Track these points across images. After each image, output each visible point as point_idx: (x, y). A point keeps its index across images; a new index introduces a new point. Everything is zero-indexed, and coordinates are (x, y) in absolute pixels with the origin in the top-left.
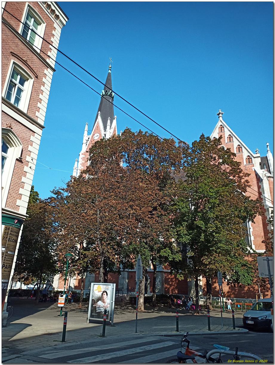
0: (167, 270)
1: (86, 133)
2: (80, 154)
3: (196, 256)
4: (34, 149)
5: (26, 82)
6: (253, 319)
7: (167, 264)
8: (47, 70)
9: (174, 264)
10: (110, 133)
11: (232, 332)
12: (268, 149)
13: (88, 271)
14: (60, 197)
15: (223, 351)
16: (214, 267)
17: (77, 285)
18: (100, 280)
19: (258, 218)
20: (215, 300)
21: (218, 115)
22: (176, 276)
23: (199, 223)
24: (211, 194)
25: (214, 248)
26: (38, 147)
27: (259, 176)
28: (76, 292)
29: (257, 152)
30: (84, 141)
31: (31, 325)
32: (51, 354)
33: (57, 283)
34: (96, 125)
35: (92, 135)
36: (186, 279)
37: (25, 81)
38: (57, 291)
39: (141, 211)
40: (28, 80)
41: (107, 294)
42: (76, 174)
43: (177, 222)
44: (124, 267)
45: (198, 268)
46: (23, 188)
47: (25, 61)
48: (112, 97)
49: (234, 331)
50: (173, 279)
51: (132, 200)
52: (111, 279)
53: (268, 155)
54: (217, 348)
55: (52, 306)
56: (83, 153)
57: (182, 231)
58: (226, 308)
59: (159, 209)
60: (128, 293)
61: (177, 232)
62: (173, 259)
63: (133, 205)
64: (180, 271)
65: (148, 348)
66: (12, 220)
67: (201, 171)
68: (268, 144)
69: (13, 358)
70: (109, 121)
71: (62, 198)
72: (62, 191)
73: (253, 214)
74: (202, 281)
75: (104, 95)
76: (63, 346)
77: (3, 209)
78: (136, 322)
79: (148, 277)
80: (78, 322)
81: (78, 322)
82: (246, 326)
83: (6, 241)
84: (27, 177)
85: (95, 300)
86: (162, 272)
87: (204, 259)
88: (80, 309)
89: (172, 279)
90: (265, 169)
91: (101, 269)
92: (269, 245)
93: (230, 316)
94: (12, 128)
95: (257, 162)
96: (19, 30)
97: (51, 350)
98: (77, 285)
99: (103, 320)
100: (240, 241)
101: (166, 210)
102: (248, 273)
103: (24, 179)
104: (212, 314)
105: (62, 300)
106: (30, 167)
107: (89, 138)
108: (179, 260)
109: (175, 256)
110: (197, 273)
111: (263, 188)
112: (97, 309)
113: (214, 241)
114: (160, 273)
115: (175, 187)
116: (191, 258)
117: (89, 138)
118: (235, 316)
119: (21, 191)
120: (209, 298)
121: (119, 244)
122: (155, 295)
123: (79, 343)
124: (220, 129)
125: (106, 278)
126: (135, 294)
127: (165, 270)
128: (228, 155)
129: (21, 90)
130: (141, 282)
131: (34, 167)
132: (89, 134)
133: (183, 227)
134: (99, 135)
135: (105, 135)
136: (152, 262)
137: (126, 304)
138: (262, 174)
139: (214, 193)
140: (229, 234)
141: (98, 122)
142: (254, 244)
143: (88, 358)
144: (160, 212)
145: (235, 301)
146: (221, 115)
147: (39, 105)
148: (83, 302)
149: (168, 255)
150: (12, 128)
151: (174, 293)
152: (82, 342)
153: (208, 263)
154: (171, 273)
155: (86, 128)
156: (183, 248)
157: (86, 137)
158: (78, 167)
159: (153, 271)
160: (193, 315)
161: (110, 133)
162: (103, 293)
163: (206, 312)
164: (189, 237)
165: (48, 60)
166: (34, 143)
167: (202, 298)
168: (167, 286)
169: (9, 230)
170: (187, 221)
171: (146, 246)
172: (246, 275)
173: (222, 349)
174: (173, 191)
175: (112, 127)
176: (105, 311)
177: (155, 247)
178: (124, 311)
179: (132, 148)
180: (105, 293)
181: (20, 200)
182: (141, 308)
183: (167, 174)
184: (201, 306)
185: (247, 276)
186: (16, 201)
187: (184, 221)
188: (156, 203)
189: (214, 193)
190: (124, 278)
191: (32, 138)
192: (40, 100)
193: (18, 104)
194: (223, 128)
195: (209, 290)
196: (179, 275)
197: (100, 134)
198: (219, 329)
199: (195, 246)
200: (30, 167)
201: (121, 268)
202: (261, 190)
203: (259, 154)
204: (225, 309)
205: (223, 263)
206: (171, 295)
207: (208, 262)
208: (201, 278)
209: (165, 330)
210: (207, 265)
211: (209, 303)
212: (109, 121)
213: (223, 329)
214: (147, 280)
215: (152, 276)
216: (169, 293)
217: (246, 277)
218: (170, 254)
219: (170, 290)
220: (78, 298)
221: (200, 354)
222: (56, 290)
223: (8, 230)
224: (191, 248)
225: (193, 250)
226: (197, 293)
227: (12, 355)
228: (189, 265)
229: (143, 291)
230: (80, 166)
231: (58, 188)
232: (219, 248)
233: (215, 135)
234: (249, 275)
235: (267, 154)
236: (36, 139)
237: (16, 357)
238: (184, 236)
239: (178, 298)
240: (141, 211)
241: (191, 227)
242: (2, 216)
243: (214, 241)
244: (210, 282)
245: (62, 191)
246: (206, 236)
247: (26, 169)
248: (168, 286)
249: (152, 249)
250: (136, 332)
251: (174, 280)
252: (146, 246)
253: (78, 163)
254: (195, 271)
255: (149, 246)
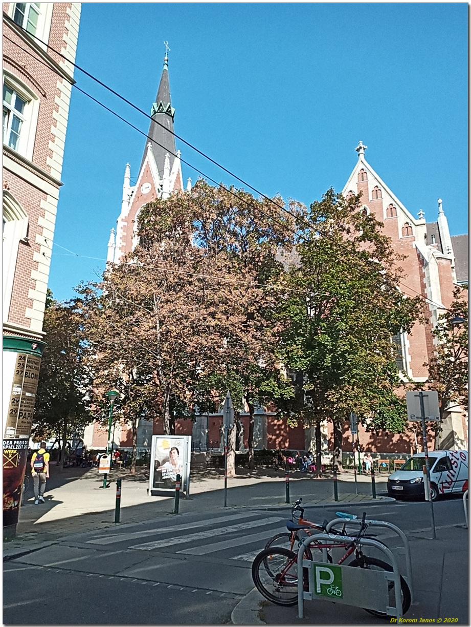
0: (272, 411)
1: (127, 182)
2: (119, 219)
3: (317, 390)
4: (48, 223)
5: (26, 105)
6: (402, 483)
7: (272, 404)
8: (62, 83)
9: (282, 404)
10: (170, 182)
11: (371, 502)
12: (441, 209)
13: (143, 416)
14: (91, 298)
15: (348, 520)
16: (344, 405)
17: (125, 440)
18: (165, 431)
19: (418, 327)
20: (348, 456)
21: (358, 150)
22: (285, 422)
23: (323, 338)
24: (342, 292)
25: (346, 377)
26: (53, 219)
27: (423, 257)
28: (123, 450)
29: (422, 216)
30: (125, 198)
31: (61, 502)
32: (103, 539)
33: (92, 436)
34: (144, 167)
35: (137, 185)
36: (301, 425)
37: (24, 103)
38: (92, 451)
39: (229, 322)
40: (29, 101)
41: (178, 452)
42: (115, 256)
43: (287, 337)
44: (202, 410)
45: (321, 409)
46: (34, 288)
47: (22, 68)
48: (171, 116)
49: (374, 501)
50: (281, 425)
51: (213, 303)
52: (181, 428)
53: (440, 219)
54: (340, 517)
55: (88, 474)
56: (124, 218)
57: (296, 351)
58: (364, 469)
59: (258, 316)
60: (208, 450)
61: (287, 353)
62: (282, 395)
63: (216, 313)
64: (293, 413)
65: (244, 526)
66: (29, 344)
67: (326, 253)
68: (440, 201)
69: (49, 546)
70: (167, 161)
71: (93, 299)
72: (94, 288)
73: (411, 320)
74: (327, 428)
75: (157, 112)
76: (117, 528)
77: (4, 325)
78: (225, 491)
79: (241, 425)
80: (137, 494)
81: (137, 494)
82: (392, 493)
83: (22, 376)
84: (39, 270)
85: (160, 462)
86: (263, 415)
87: (330, 395)
88: (133, 476)
89: (279, 425)
90: (434, 244)
91: (167, 414)
92: (433, 369)
93: (368, 479)
94: (8, 189)
95: (420, 232)
96: (9, 10)
97: (102, 534)
98: (125, 440)
99: (175, 490)
100: (388, 365)
101: (268, 319)
102: (399, 414)
103: (34, 274)
104: (339, 478)
105: (105, 463)
106: (44, 254)
107: (133, 192)
108: (290, 397)
109: (284, 391)
110: (318, 416)
111: (429, 277)
112: (163, 475)
113: (346, 366)
114: (259, 417)
115: (283, 280)
116: (308, 393)
117: (133, 192)
118: (377, 480)
119: (32, 294)
120: (338, 456)
121: (193, 375)
122: (253, 452)
123: (141, 523)
124: (361, 175)
125: (173, 428)
126: (221, 451)
127: (269, 413)
128: (369, 226)
129: (20, 119)
130: (229, 433)
131: (49, 253)
132: (133, 183)
133: (297, 345)
134: (149, 185)
135: (162, 186)
136: (247, 401)
137: (206, 467)
138: (428, 253)
139: (347, 290)
140: (370, 354)
141: (148, 162)
142: (411, 368)
143: (159, 541)
144: (259, 321)
145: (380, 457)
146: (362, 151)
147: (51, 145)
148: (136, 465)
149: (274, 390)
150: (8, 189)
151: (283, 447)
152: (146, 522)
153: (335, 400)
154: (277, 417)
155: (128, 174)
156: (297, 377)
157: (127, 189)
158: (115, 243)
159: (249, 414)
160: (312, 479)
161: (170, 182)
162: (172, 452)
163: (332, 476)
164: (306, 361)
165: (61, 64)
166: (46, 212)
167: (326, 454)
168: (271, 436)
169: (25, 359)
170: (303, 336)
171: (237, 376)
172: (396, 417)
173: (347, 517)
174: (281, 287)
175: (172, 172)
176: (178, 476)
177: (252, 377)
178: (205, 478)
179: (210, 215)
180: (175, 451)
181: (30, 309)
182: (230, 472)
183: (270, 257)
184: (325, 466)
185: (398, 420)
186: (25, 311)
187: (299, 335)
188: (254, 308)
189: (347, 290)
190: (201, 427)
191: (43, 204)
192: (53, 138)
193: (15, 144)
194: (365, 174)
195: (338, 443)
196: (291, 419)
197: (153, 185)
198: (351, 498)
199: (316, 375)
200: (44, 254)
201: (196, 410)
202: (425, 281)
203: (424, 220)
204: (362, 470)
205: (360, 399)
206: (278, 450)
207: (336, 398)
208: (325, 422)
209: (268, 502)
210: (333, 403)
211: (338, 461)
212: (167, 161)
213: (359, 499)
214: (238, 429)
215: (247, 425)
216: (275, 447)
217: (396, 420)
218: (277, 389)
219: (277, 443)
220: (132, 461)
221: (318, 525)
222: (89, 449)
223: (23, 360)
224: (310, 377)
225: (313, 381)
226: (319, 444)
227: (45, 542)
228: (306, 405)
229: (234, 447)
230: (119, 241)
231: (86, 283)
232: (353, 377)
233: (351, 186)
234: (400, 417)
235: (439, 219)
236: (50, 206)
237: (52, 544)
238: (298, 360)
239: (289, 454)
240: (229, 322)
241: (309, 345)
242: (5, 338)
243: (346, 366)
244: (339, 430)
245: (94, 288)
246: (333, 358)
247: (37, 257)
248: (274, 437)
249: (247, 380)
250: (225, 506)
251: (283, 427)
252: (237, 376)
253: (115, 237)
254: (315, 413)
255: (242, 376)
